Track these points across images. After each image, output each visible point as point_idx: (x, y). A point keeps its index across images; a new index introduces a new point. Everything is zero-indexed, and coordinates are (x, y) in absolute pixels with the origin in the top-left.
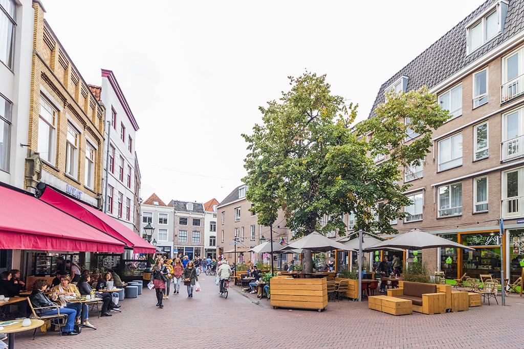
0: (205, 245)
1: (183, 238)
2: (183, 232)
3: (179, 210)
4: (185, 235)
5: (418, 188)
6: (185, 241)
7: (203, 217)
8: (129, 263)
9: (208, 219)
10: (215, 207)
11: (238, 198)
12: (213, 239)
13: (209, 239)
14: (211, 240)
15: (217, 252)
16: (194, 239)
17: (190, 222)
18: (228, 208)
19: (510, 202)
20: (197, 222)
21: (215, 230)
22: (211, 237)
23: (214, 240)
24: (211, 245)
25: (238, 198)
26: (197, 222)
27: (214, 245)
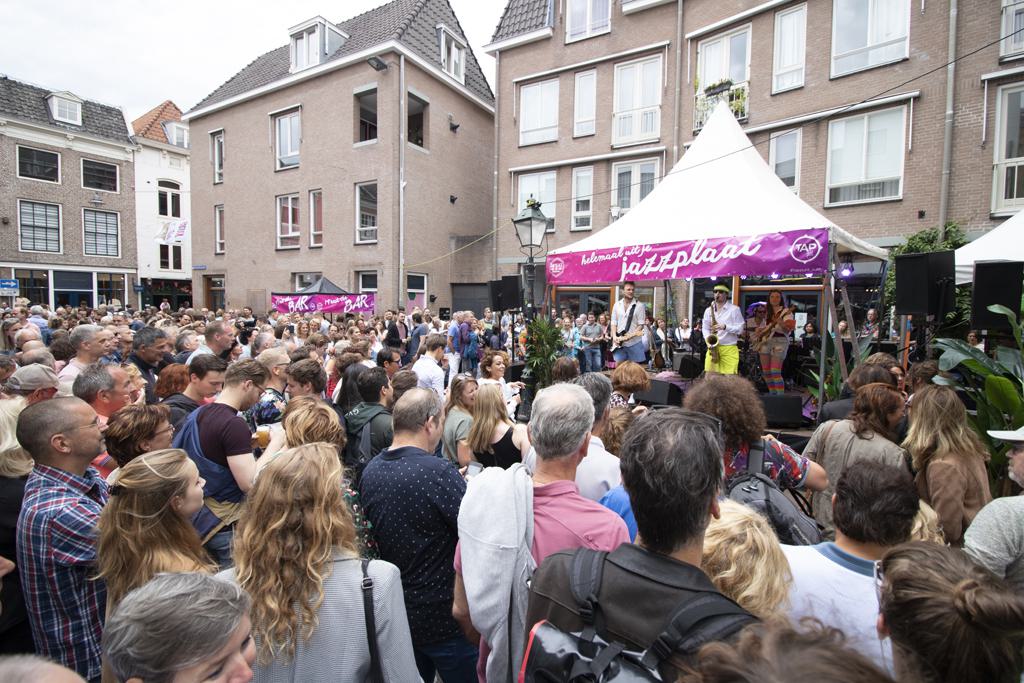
0: (142, 262)
1: (40, 234)
2: (39, 210)
3: (15, 115)
4: (52, 224)
5: (805, 113)
6: (52, 246)
7: (130, 157)
8: (337, 301)
9: (147, 170)
10: (177, 132)
11: (285, 73)
12: (170, 192)
13: (156, 189)
14: (163, 198)
15: (198, 293)
16: (91, 239)
17: (70, 173)
18: (240, 115)
19: (1011, 170)
20: (101, 175)
21: (176, 213)
22: (162, 183)
23: (176, 198)
24: (164, 264)
25: (285, 73)
26: (101, 175)
27: (178, 265)
